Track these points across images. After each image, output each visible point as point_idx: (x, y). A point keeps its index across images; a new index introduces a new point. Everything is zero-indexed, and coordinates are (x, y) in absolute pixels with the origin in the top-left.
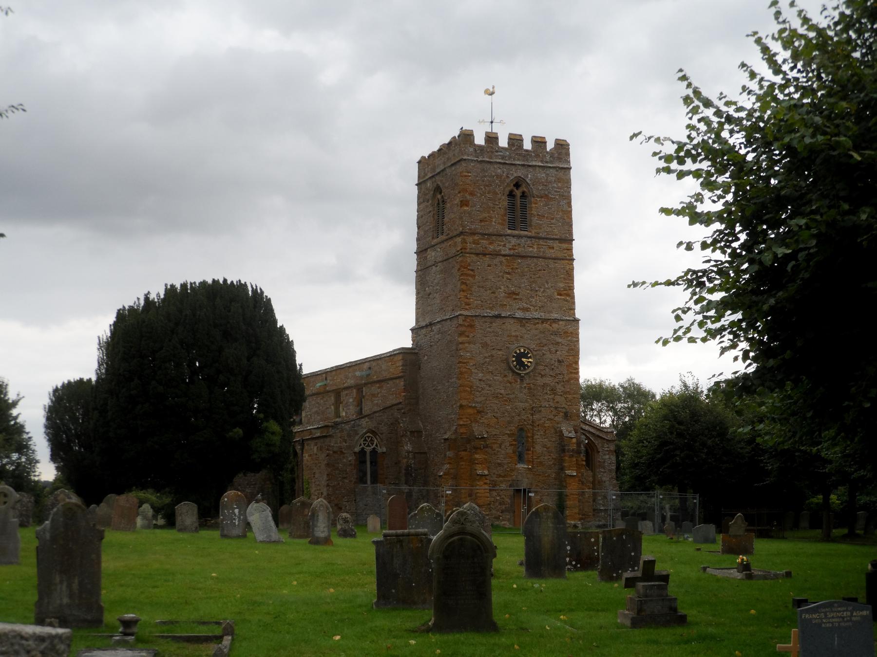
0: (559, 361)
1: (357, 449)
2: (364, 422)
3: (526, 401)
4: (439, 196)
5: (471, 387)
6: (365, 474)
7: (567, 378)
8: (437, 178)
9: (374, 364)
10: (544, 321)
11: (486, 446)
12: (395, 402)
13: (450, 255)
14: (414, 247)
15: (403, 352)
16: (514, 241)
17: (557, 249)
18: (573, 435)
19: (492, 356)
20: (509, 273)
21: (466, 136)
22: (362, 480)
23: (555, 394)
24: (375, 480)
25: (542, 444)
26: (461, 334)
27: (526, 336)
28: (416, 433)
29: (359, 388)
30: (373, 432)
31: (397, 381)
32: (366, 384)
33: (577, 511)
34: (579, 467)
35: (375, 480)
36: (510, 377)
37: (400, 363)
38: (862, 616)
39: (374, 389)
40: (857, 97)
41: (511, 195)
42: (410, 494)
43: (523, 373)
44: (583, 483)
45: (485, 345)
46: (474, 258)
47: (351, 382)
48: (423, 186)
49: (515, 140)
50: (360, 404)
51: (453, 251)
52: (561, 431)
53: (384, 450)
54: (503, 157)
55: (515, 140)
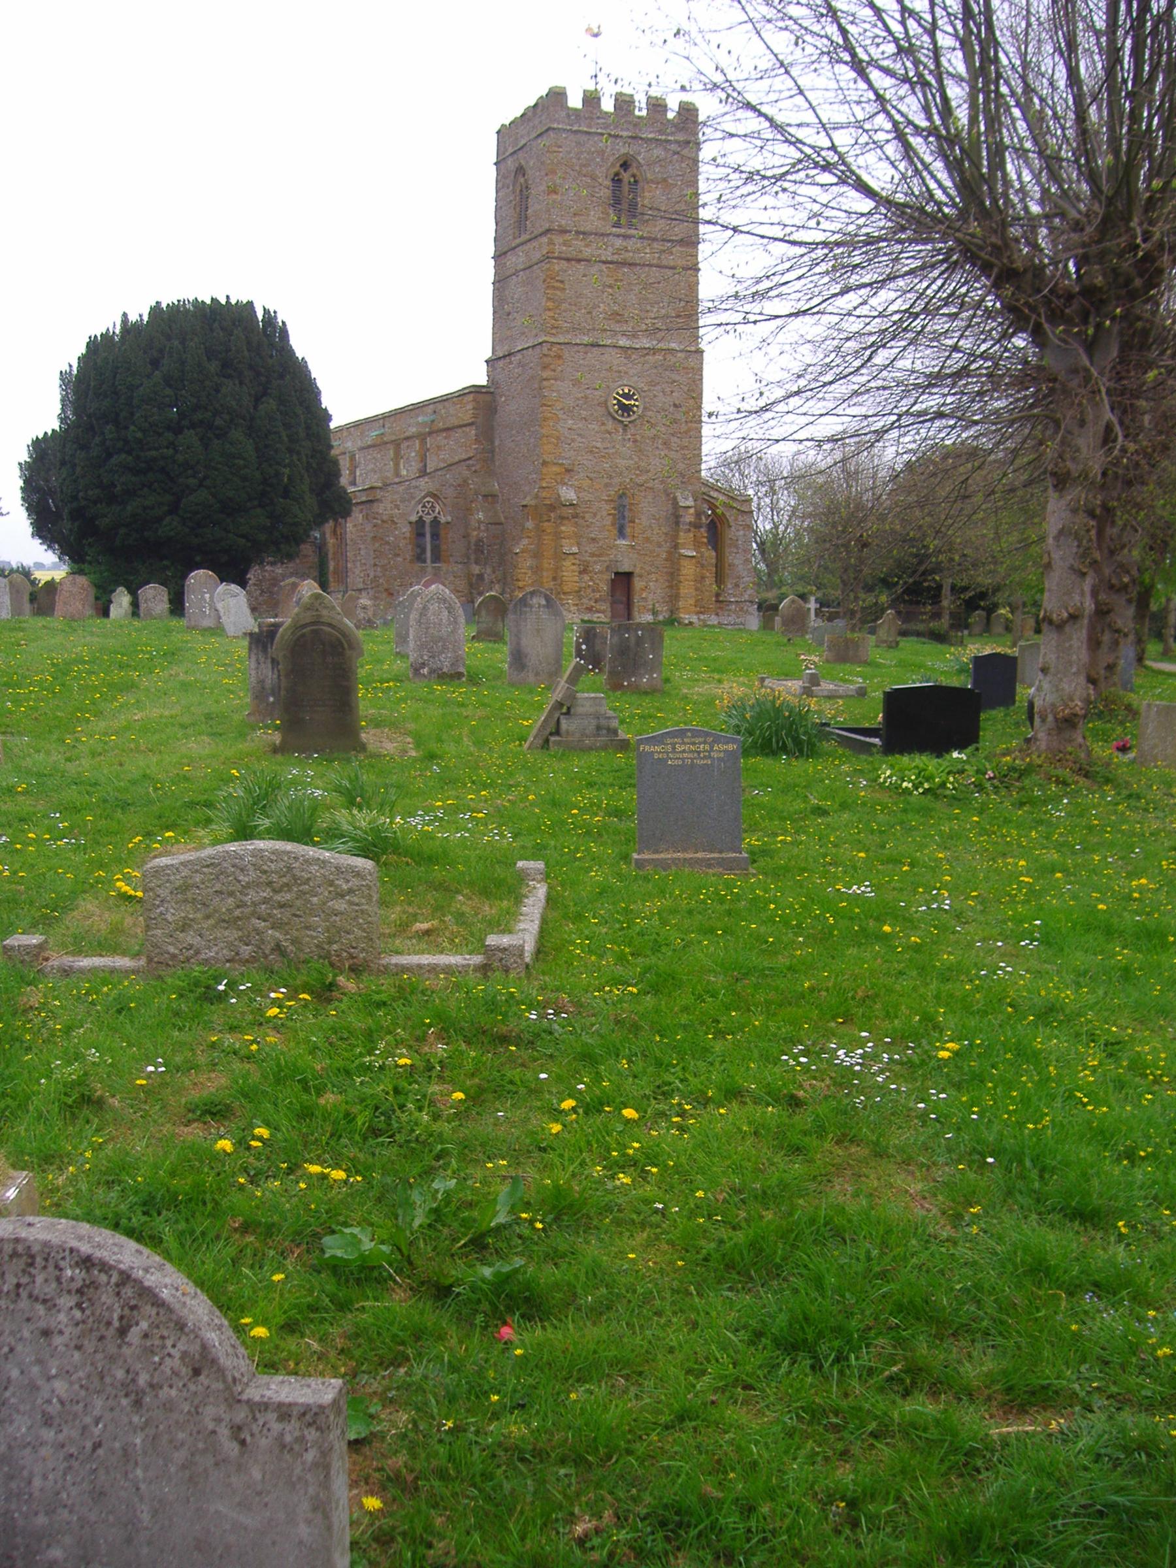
0: (675, 405)
1: (414, 518)
2: (422, 482)
3: (631, 458)
4: (522, 180)
5: (558, 438)
6: (424, 551)
7: (684, 427)
8: (520, 154)
9: (440, 406)
10: (653, 351)
11: (576, 516)
12: (464, 456)
13: (534, 260)
14: (490, 250)
15: (475, 390)
16: (619, 242)
17: (676, 257)
18: (690, 502)
19: (586, 397)
20: (610, 286)
21: (556, 96)
22: (420, 558)
23: (670, 449)
24: (437, 558)
25: (649, 514)
26: (545, 367)
27: (631, 372)
28: (490, 497)
29: (422, 437)
30: (434, 496)
31: (467, 429)
32: (430, 433)
33: (692, 602)
34: (697, 545)
35: (437, 558)
36: (610, 425)
37: (470, 406)
38: (725, 751)
39: (440, 439)
40: (1134, 335)
41: (617, 180)
42: (480, 577)
43: (626, 420)
44: (702, 566)
45: (576, 383)
46: (564, 264)
47: (413, 430)
48: (502, 166)
49: (624, 103)
50: (423, 459)
51: (537, 256)
52: (675, 498)
53: (449, 519)
54: (607, 127)
55: (624, 103)
